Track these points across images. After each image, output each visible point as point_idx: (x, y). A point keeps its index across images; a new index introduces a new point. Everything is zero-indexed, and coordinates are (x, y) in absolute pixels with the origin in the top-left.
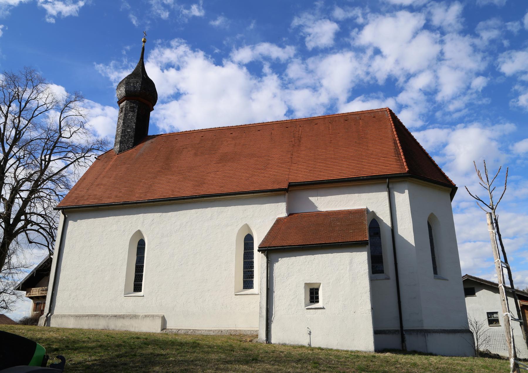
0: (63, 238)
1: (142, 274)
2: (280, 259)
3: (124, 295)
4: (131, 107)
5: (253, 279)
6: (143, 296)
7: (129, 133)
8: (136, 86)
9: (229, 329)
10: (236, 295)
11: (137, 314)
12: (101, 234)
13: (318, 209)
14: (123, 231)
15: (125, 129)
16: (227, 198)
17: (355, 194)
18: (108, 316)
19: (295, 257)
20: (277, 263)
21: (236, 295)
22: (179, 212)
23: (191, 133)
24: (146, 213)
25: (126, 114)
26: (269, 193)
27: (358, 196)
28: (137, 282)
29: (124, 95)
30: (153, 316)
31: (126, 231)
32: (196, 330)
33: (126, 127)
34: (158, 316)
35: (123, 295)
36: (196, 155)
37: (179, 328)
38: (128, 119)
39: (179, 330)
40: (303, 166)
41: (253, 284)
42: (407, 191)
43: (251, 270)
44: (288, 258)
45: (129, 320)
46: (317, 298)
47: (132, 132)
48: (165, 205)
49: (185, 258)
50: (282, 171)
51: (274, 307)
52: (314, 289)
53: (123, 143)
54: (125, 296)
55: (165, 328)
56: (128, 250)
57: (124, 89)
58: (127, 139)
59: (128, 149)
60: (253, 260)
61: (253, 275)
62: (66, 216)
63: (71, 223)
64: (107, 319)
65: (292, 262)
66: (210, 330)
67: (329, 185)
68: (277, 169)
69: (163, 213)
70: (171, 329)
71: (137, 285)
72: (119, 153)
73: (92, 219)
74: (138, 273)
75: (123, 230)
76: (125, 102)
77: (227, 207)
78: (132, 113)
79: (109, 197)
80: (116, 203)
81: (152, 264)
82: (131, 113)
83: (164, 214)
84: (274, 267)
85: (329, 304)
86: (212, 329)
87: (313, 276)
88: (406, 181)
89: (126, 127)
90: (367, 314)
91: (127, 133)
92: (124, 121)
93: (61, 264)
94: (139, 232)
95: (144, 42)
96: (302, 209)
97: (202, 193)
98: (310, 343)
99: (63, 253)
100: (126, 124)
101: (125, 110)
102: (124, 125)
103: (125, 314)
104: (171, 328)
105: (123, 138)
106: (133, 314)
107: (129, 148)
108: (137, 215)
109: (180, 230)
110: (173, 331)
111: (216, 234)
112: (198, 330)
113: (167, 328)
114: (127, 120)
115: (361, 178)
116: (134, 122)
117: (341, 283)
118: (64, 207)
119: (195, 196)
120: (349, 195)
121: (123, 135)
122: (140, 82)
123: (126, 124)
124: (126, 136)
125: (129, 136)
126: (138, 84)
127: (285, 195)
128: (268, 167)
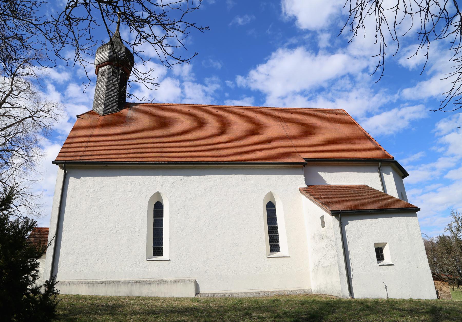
0: (64, 196)
1: (161, 237)
2: (349, 222)
3: (147, 259)
4: (114, 73)
5: (278, 243)
6: (170, 260)
7: (113, 97)
8: (120, 53)
9: (265, 291)
10: (268, 258)
11: (164, 279)
13: (327, 183)
15: (109, 92)
16: (250, 167)
17: (165, 176)
18: (129, 283)
19: (362, 220)
20: (347, 226)
21: (268, 258)
22: (202, 176)
24: (354, 172)
25: (109, 77)
26: (291, 165)
27: (357, 174)
28: (157, 245)
29: (106, 59)
30: (184, 281)
32: (232, 293)
33: (109, 90)
34: (190, 281)
35: (145, 259)
37: (213, 292)
39: (214, 294)
40: (93, 147)
41: (279, 248)
42: (391, 173)
43: (276, 234)
44: (357, 221)
45: (156, 286)
47: (116, 96)
48: (185, 168)
49: (212, 222)
50: (283, 148)
51: (351, 265)
53: (107, 105)
54: (147, 261)
55: (198, 293)
58: (111, 102)
60: (277, 225)
61: (279, 240)
62: (67, 172)
63: (72, 180)
64: (129, 285)
65: (360, 225)
66: (247, 293)
68: (126, 146)
69: (185, 177)
70: (206, 294)
71: (157, 249)
72: (103, 114)
73: (100, 177)
76: (107, 67)
77: (251, 175)
78: (115, 78)
80: (165, 163)
81: (177, 227)
82: (114, 78)
83: (186, 178)
84: (345, 229)
86: (249, 292)
89: (109, 90)
91: (111, 97)
92: (108, 85)
93: (63, 224)
94: (158, 194)
96: (315, 182)
98: (388, 296)
99: (64, 212)
100: (109, 88)
101: (108, 74)
102: (107, 88)
103: (149, 279)
104: (205, 292)
105: (107, 101)
106: (159, 279)
107: (113, 112)
108: (155, 177)
109: (204, 194)
110: (208, 295)
112: (235, 293)
113: (200, 292)
114: (111, 84)
115: (360, 160)
118: (66, 162)
119: (219, 163)
120: (350, 173)
123: (109, 88)
124: (109, 99)
125: (113, 99)
126: (122, 51)
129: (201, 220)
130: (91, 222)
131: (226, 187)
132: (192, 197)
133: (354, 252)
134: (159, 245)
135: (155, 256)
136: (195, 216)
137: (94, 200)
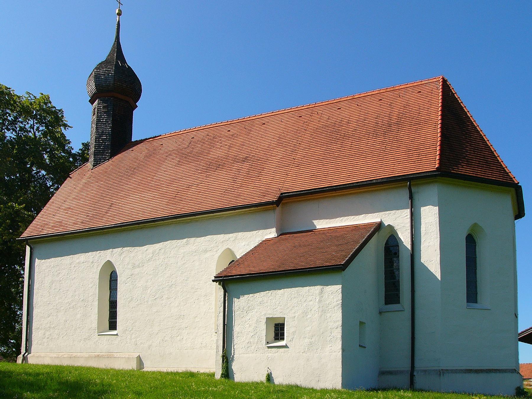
0: (32, 273)
12: (69, 267)
14: (92, 262)
23: (180, 134)
31: (95, 262)
36: (179, 163)
38: (102, 123)
46: (283, 334)
52: (279, 325)
54: (98, 335)
56: (98, 284)
57: (94, 84)
59: (104, 161)
67: (334, 194)
74: (112, 309)
75: (91, 262)
79: (75, 224)
81: (124, 299)
85: (293, 341)
87: (276, 309)
88: (436, 182)
90: (337, 353)
95: (119, 14)
97: (176, 212)
109: (152, 258)
111: (193, 262)
114: (101, 124)
116: (110, 126)
117: (308, 317)
121: (97, 145)
122: (113, 72)
127: (274, 209)
128: (262, 174)
129: (148, 289)
130: (53, 298)
131: (176, 247)
132: (140, 263)
133: (238, 329)
134: (114, 319)
135: (111, 330)
136: (142, 286)
137: (55, 275)
